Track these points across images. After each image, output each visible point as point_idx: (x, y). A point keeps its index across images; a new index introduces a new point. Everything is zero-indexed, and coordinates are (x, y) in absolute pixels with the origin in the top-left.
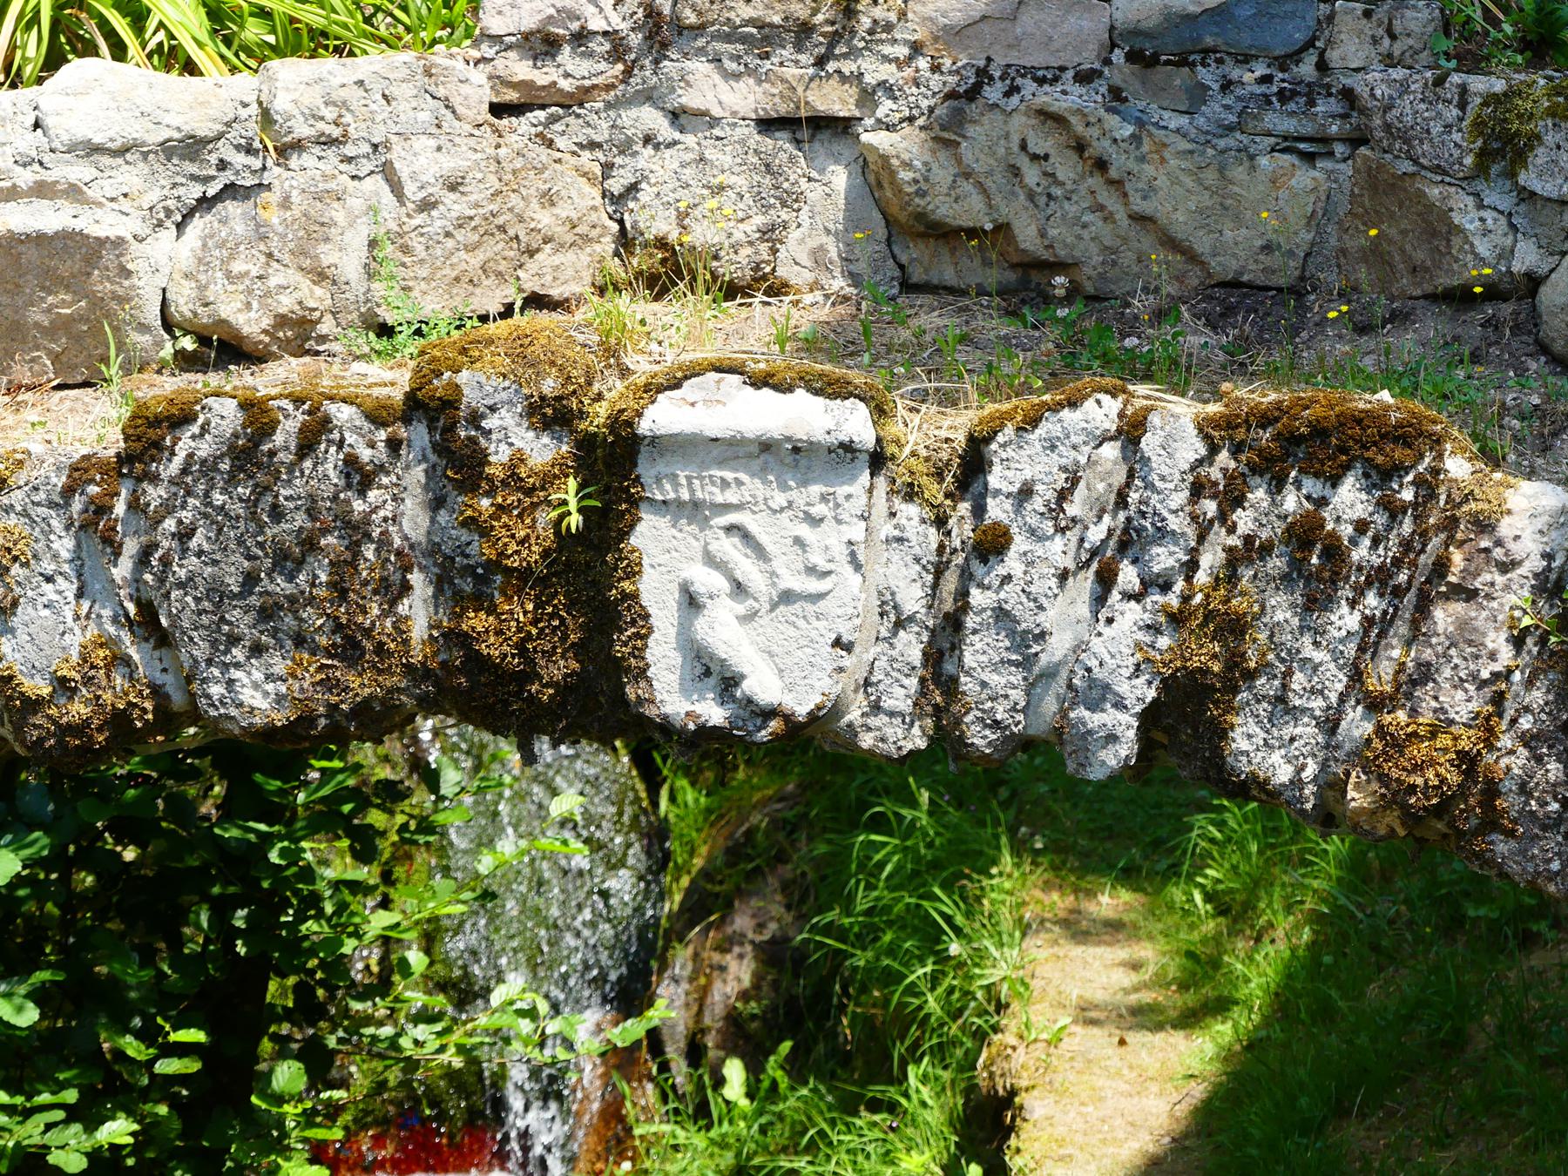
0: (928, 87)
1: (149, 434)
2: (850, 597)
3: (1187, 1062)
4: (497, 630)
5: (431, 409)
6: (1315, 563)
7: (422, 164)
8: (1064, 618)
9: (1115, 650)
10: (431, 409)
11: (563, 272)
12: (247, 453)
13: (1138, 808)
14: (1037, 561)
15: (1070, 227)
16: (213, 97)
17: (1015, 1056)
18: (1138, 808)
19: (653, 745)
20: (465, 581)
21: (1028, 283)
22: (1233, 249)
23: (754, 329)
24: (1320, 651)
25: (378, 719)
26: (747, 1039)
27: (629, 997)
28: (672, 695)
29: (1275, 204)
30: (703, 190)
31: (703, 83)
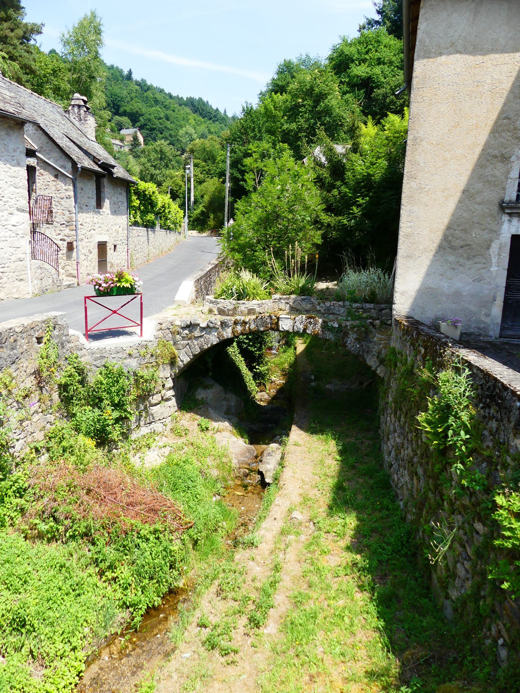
0: (293, 301)
1: (257, 317)
2: (289, 325)
3: (305, 345)
4: (273, 326)
5: (270, 316)
6: (310, 323)
7: (269, 305)
8: (299, 326)
9: (301, 327)
10: (270, 316)
11: (276, 310)
12: (261, 318)
13: (302, 334)
14: (298, 323)
15: (299, 307)
16: (260, 302)
17: (297, 345)
18: (302, 334)
19: (280, 331)
20: (271, 324)
21: (297, 310)
22: (307, 309)
23: (285, 312)
24: (311, 327)
25: (267, 330)
26: (284, 345)
27: (279, 342)
28: (281, 329)
29: (309, 306)
30: (282, 306)
31: (282, 301)
